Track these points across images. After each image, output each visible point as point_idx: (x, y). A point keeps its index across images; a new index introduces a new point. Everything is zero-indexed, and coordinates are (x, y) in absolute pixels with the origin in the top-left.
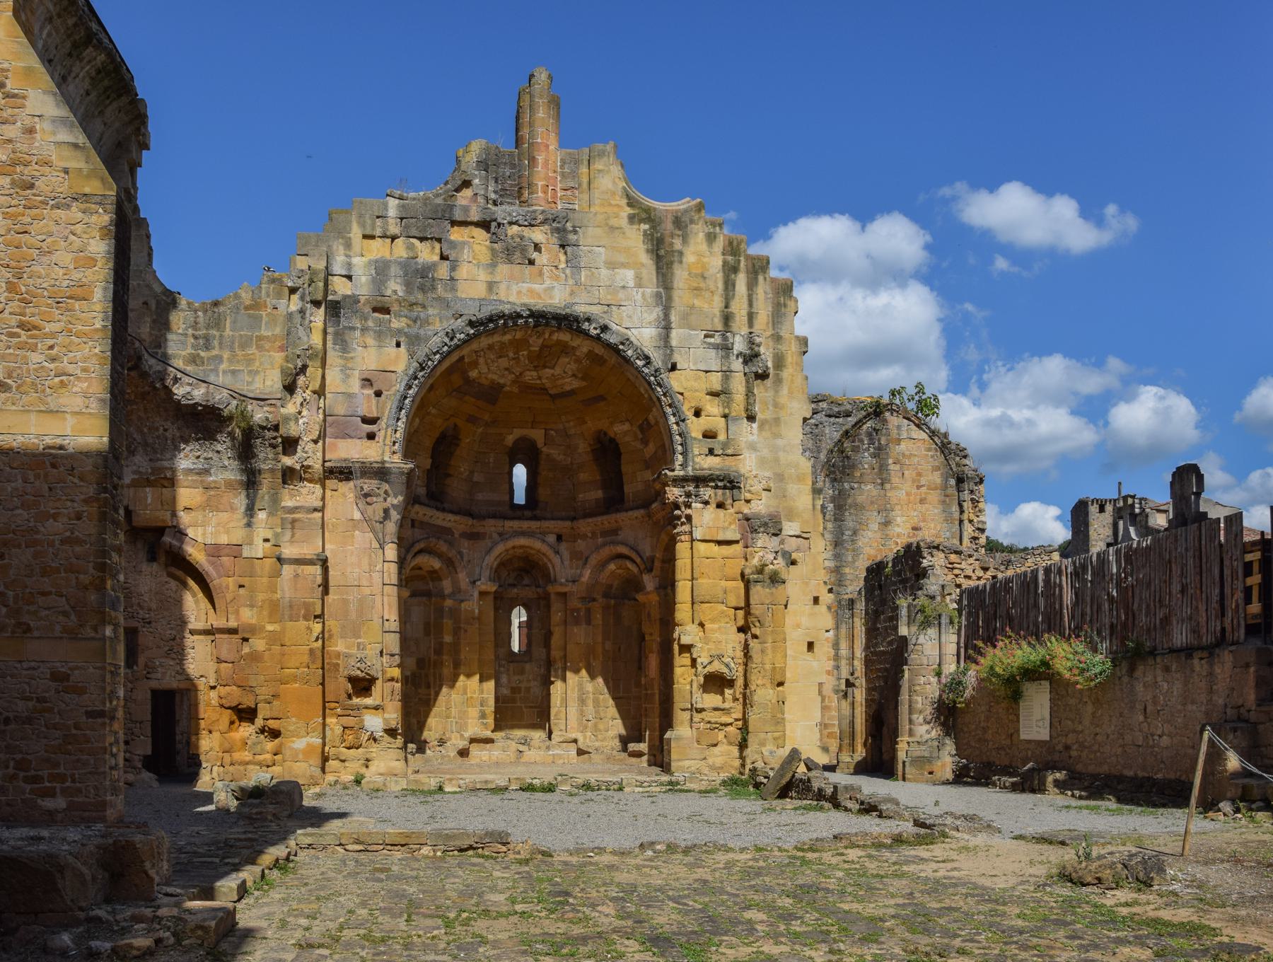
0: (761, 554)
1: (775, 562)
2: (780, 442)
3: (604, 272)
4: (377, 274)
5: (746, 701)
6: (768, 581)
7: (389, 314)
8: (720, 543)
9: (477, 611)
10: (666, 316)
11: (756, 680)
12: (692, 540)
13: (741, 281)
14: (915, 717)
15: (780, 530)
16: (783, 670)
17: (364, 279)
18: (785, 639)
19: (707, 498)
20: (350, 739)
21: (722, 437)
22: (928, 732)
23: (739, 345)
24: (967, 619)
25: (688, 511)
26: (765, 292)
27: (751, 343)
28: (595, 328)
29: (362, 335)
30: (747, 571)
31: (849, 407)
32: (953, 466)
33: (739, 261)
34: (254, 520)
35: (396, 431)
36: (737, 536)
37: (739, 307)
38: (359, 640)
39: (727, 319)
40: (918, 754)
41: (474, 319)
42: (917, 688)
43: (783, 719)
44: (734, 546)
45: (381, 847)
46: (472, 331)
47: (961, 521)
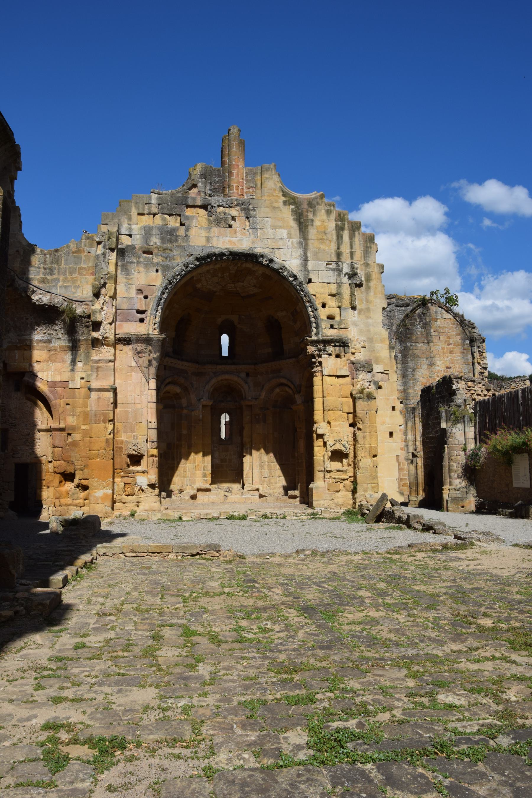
0: (361, 383)
1: (369, 387)
2: (370, 321)
3: (270, 231)
4: (146, 233)
5: (355, 466)
6: (366, 398)
7: (152, 254)
8: (338, 377)
9: (201, 416)
10: (305, 254)
11: (361, 454)
12: (323, 375)
13: (346, 235)
14: (452, 474)
15: (372, 369)
16: (376, 448)
17: (138, 236)
18: (376, 431)
19: (330, 352)
20: (128, 490)
21: (337, 318)
22: (460, 483)
23: (346, 269)
24: (479, 419)
25: (320, 359)
26: (359, 241)
27: (352, 267)
28: (266, 261)
29: (137, 266)
30: (354, 392)
31: (408, 301)
32: (468, 333)
33: (344, 224)
34: (75, 367)
35: (156, 317)
36: (347, 373)
37: (345, 249)
38: (134, 434)
39: (339, 255)
40: (455, 496)
41: (199, 256)
42: (453, 458)
43: (377, 476)
44: (346, 378)
45: (146, 554)
46: (198, 263)
47: (473, 364)
